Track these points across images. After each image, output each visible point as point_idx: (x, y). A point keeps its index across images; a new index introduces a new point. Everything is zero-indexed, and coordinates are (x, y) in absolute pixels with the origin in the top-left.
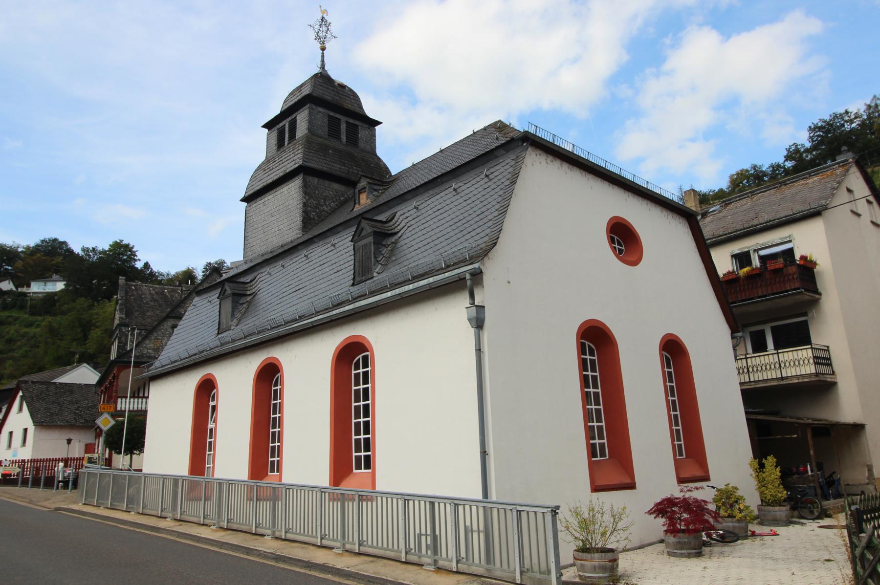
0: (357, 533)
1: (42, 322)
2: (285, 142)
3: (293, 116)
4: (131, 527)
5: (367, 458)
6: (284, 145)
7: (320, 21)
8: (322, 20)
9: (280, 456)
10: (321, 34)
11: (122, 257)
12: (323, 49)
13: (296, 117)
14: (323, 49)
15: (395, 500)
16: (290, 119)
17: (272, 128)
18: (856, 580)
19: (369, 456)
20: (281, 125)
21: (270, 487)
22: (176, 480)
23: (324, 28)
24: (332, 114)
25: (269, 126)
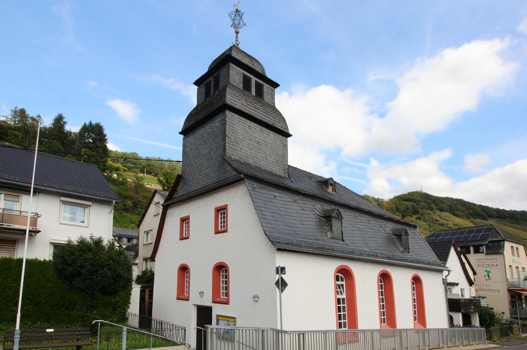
0: (259, 339)
1: (13, 139)
2: (210, 92)
3: (218, 72)
4: (40, 131)
5: (339, 303)
6: (210, 94)
7: (235, 12)
8: (236, 11)
9: (336, 291)
10: (238, 18)
11: (95, 247)
12: (237, 33)
13: (219, 73)
14: (237, 33)
15: (320, 334)
16: (215, 75)
17: (200, 86)
18: (3, 260)
19: (414, 309)
20: (206, 82)
21: (350, 332)
22: (442, 330)
23: (238, 18)
24: (246, 73)
25: (197, 83)
